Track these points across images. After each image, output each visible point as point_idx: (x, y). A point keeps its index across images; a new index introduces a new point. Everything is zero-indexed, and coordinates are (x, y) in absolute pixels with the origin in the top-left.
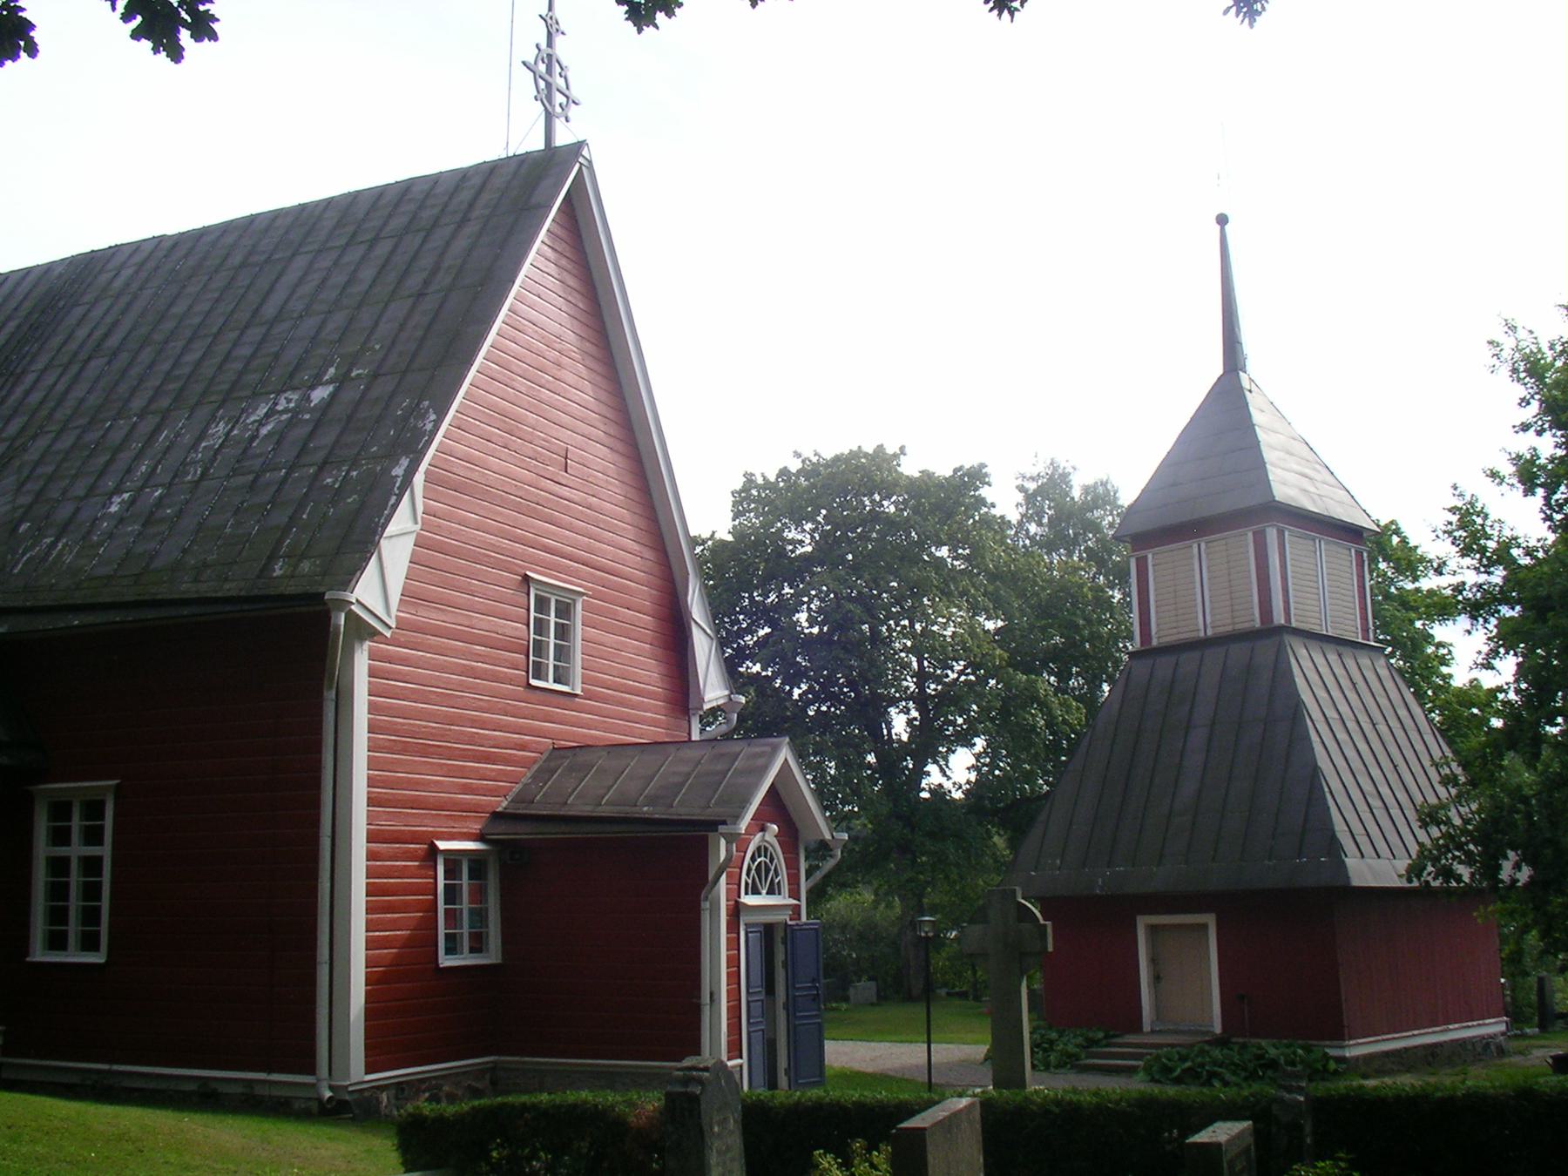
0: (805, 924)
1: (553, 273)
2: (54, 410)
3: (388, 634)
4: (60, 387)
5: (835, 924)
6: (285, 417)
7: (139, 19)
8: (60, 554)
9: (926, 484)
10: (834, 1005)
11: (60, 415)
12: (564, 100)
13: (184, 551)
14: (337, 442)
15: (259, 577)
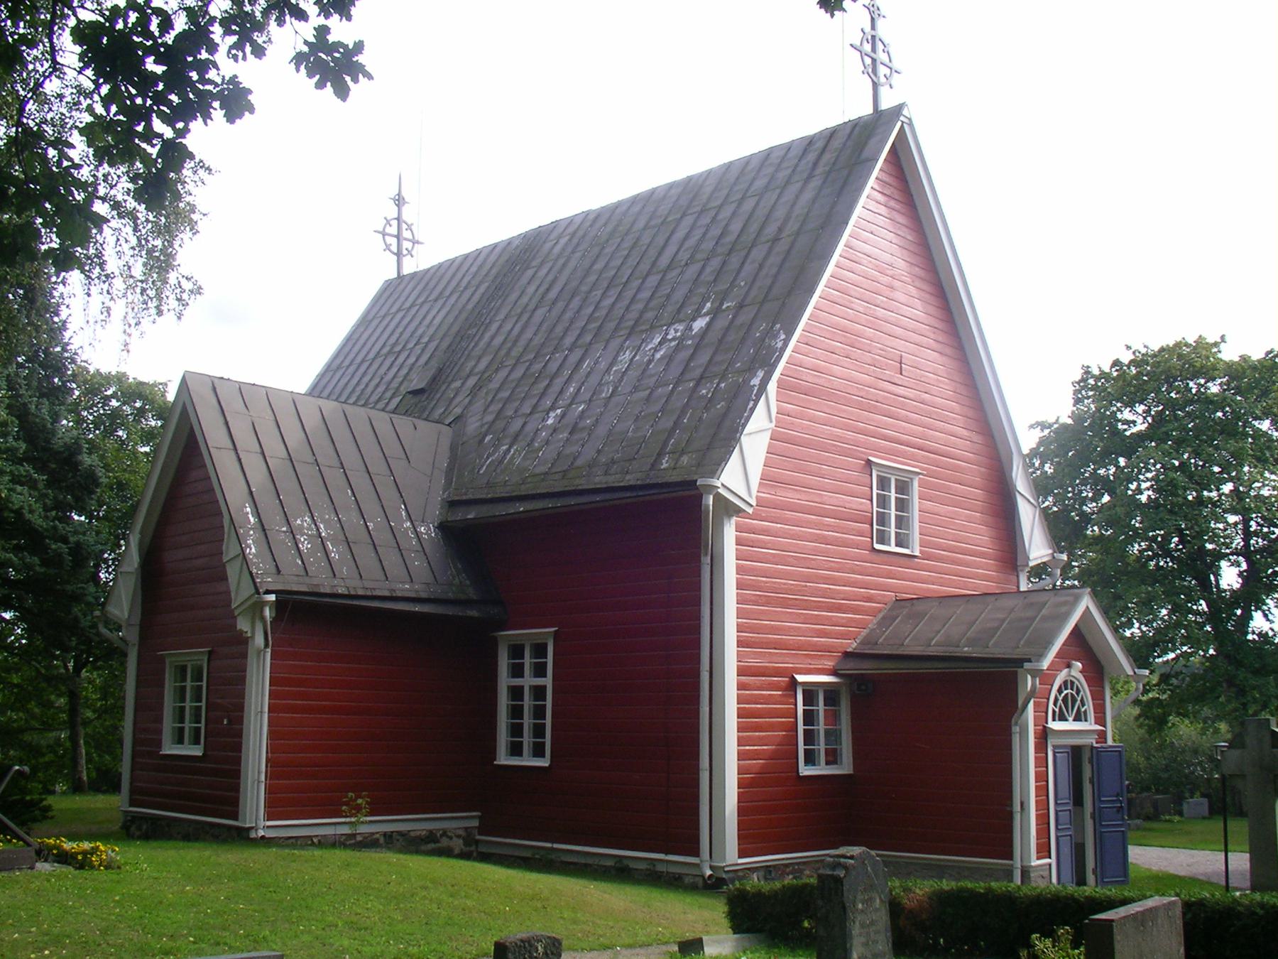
0: (1111, 747)
1: (883, 213)
2: (510, 350)
3: (750, 511)
4: (516, 332)
5: (1187, 748)
6: (673, 344)
7: (318, 77)
8: (513, 458)
9: (1243, 367)
10: (1167, 817)
11: (515, 353)
12: (887, 71)
13: (599, 452)
14: (710, 361)
15: (650, 469)
